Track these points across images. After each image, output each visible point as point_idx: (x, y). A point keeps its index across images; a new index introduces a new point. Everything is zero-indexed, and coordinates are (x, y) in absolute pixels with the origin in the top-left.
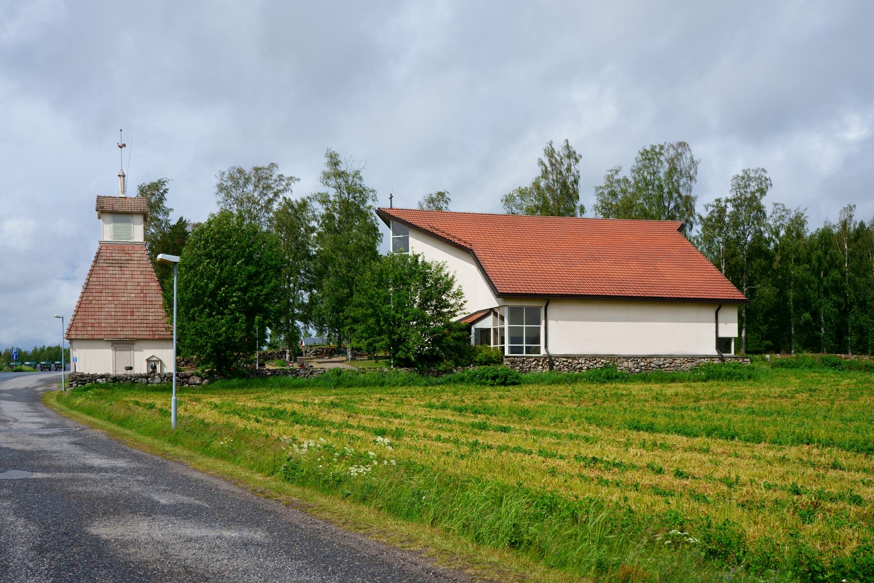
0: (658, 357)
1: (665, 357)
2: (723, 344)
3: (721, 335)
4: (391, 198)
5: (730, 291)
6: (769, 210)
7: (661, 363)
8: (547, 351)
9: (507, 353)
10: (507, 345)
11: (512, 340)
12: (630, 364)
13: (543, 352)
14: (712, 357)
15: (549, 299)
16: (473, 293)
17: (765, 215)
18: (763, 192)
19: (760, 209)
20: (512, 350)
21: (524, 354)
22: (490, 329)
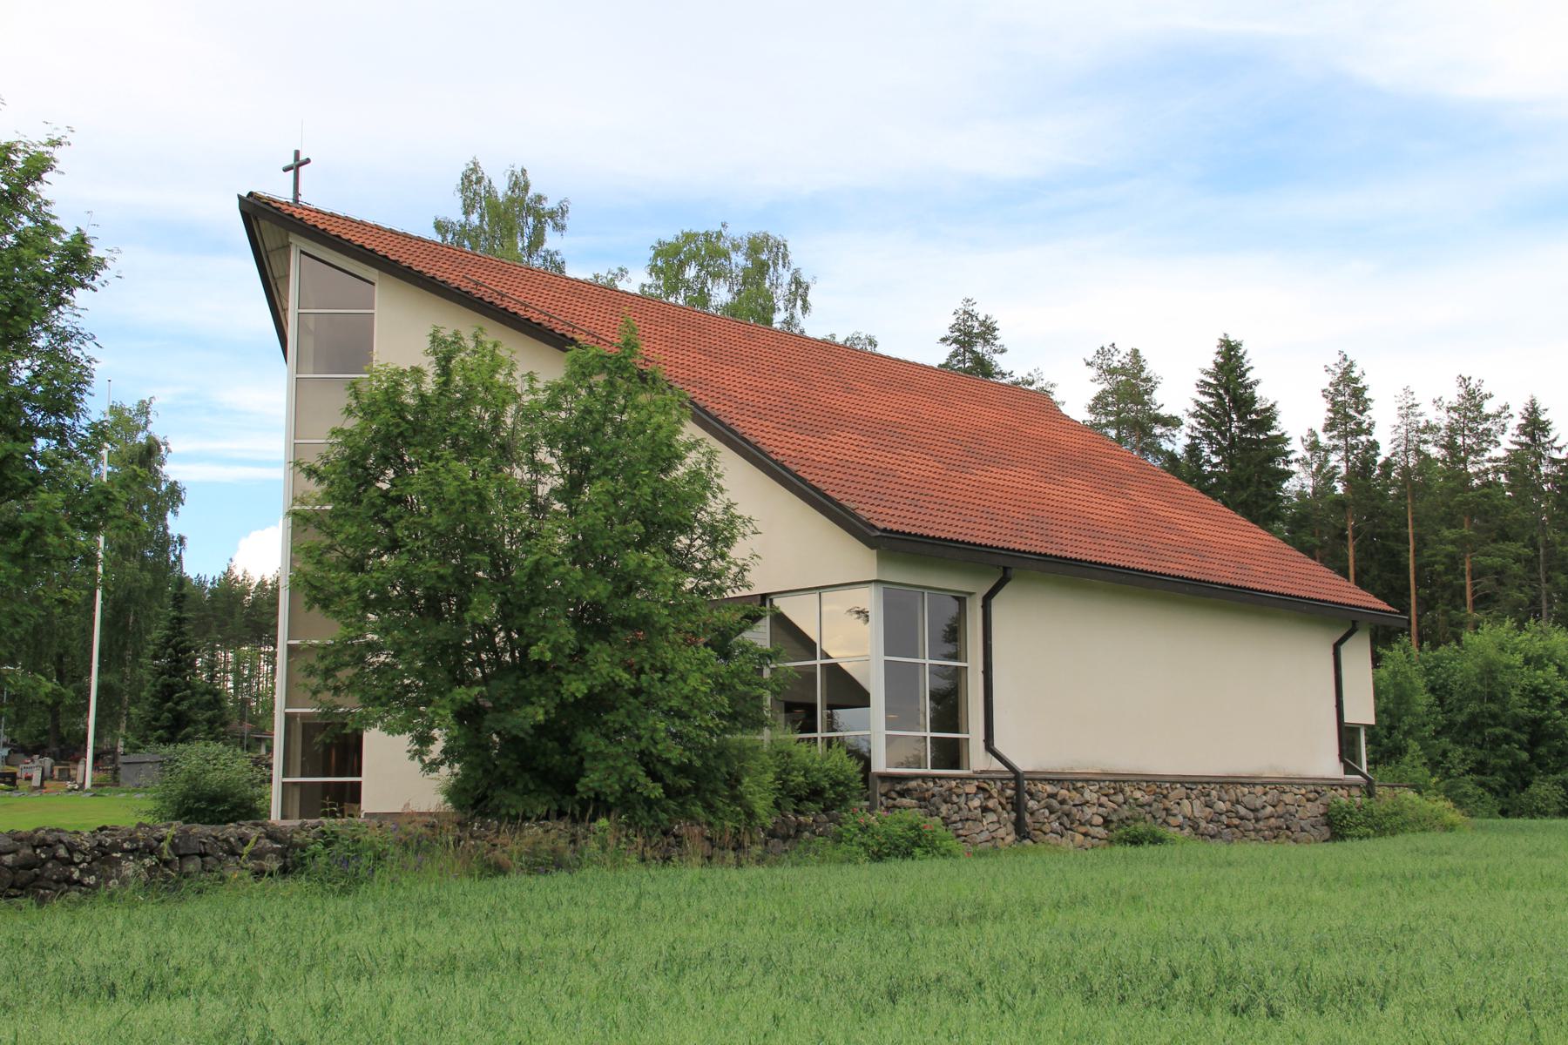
0: (1250, 782)
3: (1349, 718)
15: (1004, 567)
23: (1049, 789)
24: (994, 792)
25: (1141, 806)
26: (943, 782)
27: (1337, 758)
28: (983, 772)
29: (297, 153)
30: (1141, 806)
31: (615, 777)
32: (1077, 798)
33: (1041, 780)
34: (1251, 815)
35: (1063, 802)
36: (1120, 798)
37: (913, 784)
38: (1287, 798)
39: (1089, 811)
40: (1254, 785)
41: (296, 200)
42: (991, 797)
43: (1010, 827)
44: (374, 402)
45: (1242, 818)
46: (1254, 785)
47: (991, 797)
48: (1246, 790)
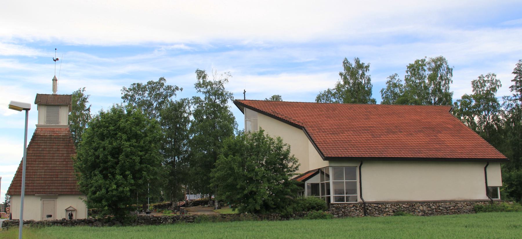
0: (445, 202)
1: (450, 202)
2: (491, 192)
3: (489, 185)
5: (493, 153)
7: (447, 206)
9: (332, 201)
10: (332, 195)
11: (336, 192)
13: (359, 200)
15: (362, 161)
16: (305, 157)
18: (494, 89)
19: (494, 100)
21: (345, 202)
22: (318, 184)
32: (384, 207)
35: (379, 208)
36: (398, 206)
38: (458, 205)
39: (387, 209)
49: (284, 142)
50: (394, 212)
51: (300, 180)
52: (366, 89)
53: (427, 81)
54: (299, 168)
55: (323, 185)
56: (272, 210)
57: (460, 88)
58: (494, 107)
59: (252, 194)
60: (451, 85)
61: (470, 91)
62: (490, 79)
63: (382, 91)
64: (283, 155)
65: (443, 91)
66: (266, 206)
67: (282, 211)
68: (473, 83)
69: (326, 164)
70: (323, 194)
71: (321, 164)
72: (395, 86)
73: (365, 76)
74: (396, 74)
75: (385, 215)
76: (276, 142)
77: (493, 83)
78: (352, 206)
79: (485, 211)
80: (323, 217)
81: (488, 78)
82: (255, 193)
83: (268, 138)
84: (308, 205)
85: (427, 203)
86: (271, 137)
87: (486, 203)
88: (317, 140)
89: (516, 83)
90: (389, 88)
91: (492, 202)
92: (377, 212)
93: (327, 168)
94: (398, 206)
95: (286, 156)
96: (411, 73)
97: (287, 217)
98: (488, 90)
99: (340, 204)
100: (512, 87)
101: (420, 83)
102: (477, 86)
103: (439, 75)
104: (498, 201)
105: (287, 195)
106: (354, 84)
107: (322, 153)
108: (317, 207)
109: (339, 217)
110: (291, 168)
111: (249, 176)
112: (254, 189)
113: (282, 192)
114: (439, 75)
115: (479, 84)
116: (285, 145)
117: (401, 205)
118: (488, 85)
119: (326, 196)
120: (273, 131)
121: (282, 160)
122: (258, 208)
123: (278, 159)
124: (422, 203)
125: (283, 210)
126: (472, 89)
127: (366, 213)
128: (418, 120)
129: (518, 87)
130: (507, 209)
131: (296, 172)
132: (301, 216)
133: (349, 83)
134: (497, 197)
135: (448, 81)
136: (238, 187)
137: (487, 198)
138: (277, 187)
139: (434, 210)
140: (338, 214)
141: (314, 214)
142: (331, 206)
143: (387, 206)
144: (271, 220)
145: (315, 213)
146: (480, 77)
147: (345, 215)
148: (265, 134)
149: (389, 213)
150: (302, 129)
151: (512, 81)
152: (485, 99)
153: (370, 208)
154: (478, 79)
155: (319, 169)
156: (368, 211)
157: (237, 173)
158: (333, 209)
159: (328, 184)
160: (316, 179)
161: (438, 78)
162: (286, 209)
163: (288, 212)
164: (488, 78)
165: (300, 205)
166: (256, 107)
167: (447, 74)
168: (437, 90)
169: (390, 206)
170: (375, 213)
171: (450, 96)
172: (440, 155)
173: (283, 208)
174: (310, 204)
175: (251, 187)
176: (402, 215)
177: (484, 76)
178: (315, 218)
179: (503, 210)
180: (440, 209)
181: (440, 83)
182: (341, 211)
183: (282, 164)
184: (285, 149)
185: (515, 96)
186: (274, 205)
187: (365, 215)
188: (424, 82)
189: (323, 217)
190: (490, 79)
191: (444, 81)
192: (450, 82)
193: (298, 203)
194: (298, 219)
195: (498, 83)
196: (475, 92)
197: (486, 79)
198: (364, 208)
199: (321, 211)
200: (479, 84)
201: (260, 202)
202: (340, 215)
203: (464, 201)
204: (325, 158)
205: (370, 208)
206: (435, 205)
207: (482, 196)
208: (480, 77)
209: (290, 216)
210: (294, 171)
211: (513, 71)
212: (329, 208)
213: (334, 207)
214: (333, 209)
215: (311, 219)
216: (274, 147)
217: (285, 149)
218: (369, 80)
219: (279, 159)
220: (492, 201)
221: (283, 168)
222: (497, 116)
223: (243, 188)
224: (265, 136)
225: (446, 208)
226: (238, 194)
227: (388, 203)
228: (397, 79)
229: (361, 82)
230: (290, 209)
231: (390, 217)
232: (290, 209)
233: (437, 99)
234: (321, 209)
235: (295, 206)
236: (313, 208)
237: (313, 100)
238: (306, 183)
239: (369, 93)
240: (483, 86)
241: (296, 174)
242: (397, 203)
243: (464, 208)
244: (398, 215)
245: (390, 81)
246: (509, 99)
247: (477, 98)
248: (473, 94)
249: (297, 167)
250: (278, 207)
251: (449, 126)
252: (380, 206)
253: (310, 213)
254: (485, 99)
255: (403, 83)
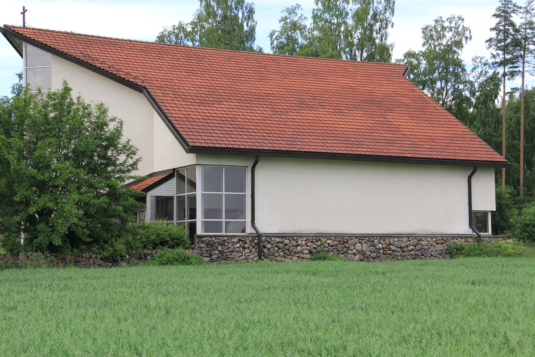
0: (399, 236)
1: (409, 236)
2: (477, 219)
3: (474, 208)
4: (23, 13)
5: (485, 152)
6: (468, 64)
7: (403, 245)
8: (255, 228)
9: (199, 231)
10: (199, 219)
11: (207, 213)
12: (365, 247)
13: (249, 230)
14: (464, 237)
15: (257, 156)
16: (152, 146)
17: (464, 70)
18: (459, 44)
19: (458, 64)
20: (207, 226)
21: (224, 233)
22: (172, 198)
23: (278, 240)
24: (248, 242)
25: (332, 246)
26: (220, 238)
27: (468, 226)
28: (250, 234)
29: (24, 7)
30: (332, 246)
31: (47, 238)
32: (294, 243)
33: (274, 237)
34: (399, 250)
35: (286, 245)
36: (319, 243)
37: (205, 239)
38: (422, 243)
39: (299, 248)
40: (402, 237)
41: (24, 26)
42: (246, 243)
43: (256, 254)
44: (55, 94)
45: (393, 251)
46: (402, 237)
47: (246, 243)
48: (396, 240)
49: (110, 114)
50: (311, 252)
51: (137, 189)
52: (246, 28)
53: (350, 21)
54: (139, 165)
55: (181, 199)
56: (84, 247)
57: (404, 39)
58: (457, 76)
59: (45, 213)
60: (389, 30)
61: (418, 47)
62: (453, 25)
63: (271, 35)
64: (107, 139)
65: (377, 41)
66: (72, 238)
67: (103, 249)
68: (425, 30)
69: (190, 159)
70: (181, 216)
71: (181, 159)
72: (295, 26)
73: (245, 5)
74: (298, 6)
75: (294, 258)
76: (95, 113)
77: (457, 33)
78: (236, 240)
79: (468, 255)
80: (184, 260)
81: (450, 23)
82: (50, 212)
83: (79, 104)
84: (154, 237)
85: (369, 238)
86: (87, 102)
87: (469, 240)
88: (173, 115)
89: (498, 34)
90: (284, 30)
91: (479, 239)
92: (281, 254)
93: (191, 168)
94: (319, 243)
95: (112, 141)
96: (323, 5)
97: (113, 260)
98: (448, 46)
99: (215, 236)
100: (490, 40)
101: (339, 25)
102: (431, 36)
103: (371, 12)
104: (489, 237)
105: (114, 216)
106: (225, 17)
107: (184, 140)
108: (174, 242)
109: (212, 261)
110: (122, 164)
111: (40, 177)
112: (50, 205)
113: (105, 211)
114: (371, 12)
115: (434, 34)
116: (113, 120)
117: (323, 240)
118: (449, 35)
119: (187, 221)
120: (90, 91)
121: (106, 148)
122: (57, 242)
123: (98, 146)
124: (361, 238)
125: (106, 246)
126: (423, 41)
127: (261, 255)
128: (351, 88)
129: (500, 41)
130: (505, 252)
131: (133, 173)
132: (142, 258)
133: (215, 15)
134: (486, 231)
135: (386, 23)
136: (17, 198)
137: (469, 232)
138: (96, 201)
139: (381, 251)
140: (211, 256)
141: (168, 255)
142: (197, 240)
143: (300, 242)
144: (85, 266)
145: (168, 253)
146: (436, 21)
147: (224, 257)
148: (74, 95)
149: (301, 255)
150: (141, 92)
151: (491, 29)
152: (443, 59)
153: (269, 246)
154: (434, 24)
155: (174, 170)
156: (265, 250)
157: (16, 171)
158: (202, 245)
159: (193, 199)
160: (168, 189)
161: (369, 17)
162: (112, 245)
163: (116, 251)
164: (450, 23)
165: (139, 237)
166: (49, 44)
167: (386, 10)
168: (368, 39)
169: (304, 243)
170: (277, 254)
171: (388, 50)
172: (341, 150)
173: (106, 242)
174: (158, 235)
175: (44, 201)
176: (325, 258)
177: (444, 19)
178: (170, 262)
179: (499, 253)
180: (390, 250)
181: (372, 26)
182: (217, 251)
183: (105, 157)
184: (112, 126)
185: (494, 56)
186: (89, 236)
187: (260, 258)
188: (345, 23)
189: (185, 261)
190: (453, 25)
191: (378, 24)
192: (390, 26)
193: (135, 234)
194: (136, 264)
195: (467, 34)
196: (426, 47)
197: (446, 24)
198: (258, 244)
199: (179, 250)
200: (434, 34)
201: (63, 230)
202: (214, 257)
203: (433, 236)
204: (191, 149)
205: (269, 246)
206: (382, 241)
207: (461, 226)
208: (436, 21)
209: (119, 258)
210: (128, 171)
211: (494, 12)
212: (193, 244)
213: (202, 242)
214: (202, 245)
215: (162, 264)
216: (91, 123)
217: (112, 126)
218: (251, 11)
219: (98, 149)
220: (479, 236)
221: (108, 165)
222: (461, 92)
223: (27, 203)
224: (75, 101)
225: (401, 248)
226: (16, 212)
227: (300, 236)
228: (299, 15)
229: (236, 16)
230: (120, 246)
231: (305, 262)
232: (120, 246)
233: (365, 55)
234: (178, 245)
235: (130, 238)
236: (163, 243)
237: (152, 38)
238: (150, 196)
239: (251, 35)
240: (441, 37)
241: (132, 177)
242: (318, 237)
243: (432, 248)
244: (319, 259)
245: (286, 18)
246: (483, 61)
247: (430, 56)
248: (423, 49)
249: (135, 163)
250: (96, 240)
251: (405, 100)
252: (287, 241)
253: (160, 251)
254: (443, 59)
255: (309, 23)
